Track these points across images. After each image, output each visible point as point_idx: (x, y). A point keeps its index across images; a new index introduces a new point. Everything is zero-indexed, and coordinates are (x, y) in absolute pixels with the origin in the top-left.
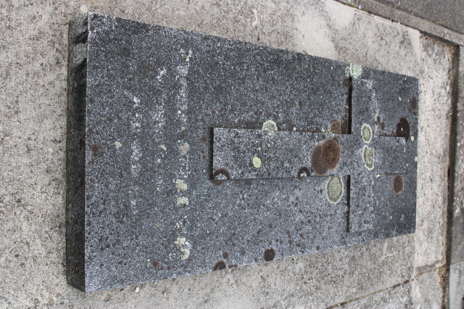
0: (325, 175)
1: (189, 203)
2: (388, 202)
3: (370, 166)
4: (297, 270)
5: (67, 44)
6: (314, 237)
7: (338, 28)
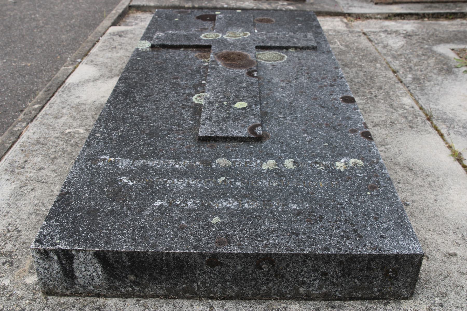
1: (292, 158)
5: (75, 298)
7: (99, 74)
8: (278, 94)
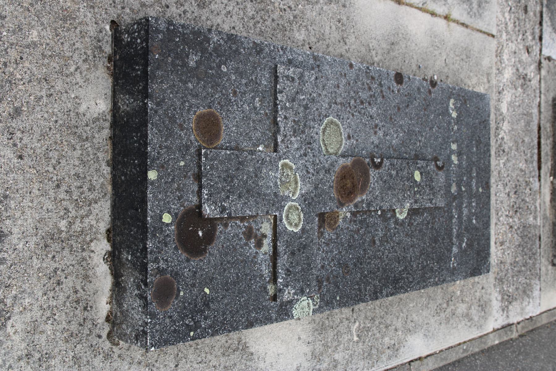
0: (353, 158)
2: (233, 99)
3: (285, 165)
4: (303, 31)
6: (356, 82)
8: (394, 141)
